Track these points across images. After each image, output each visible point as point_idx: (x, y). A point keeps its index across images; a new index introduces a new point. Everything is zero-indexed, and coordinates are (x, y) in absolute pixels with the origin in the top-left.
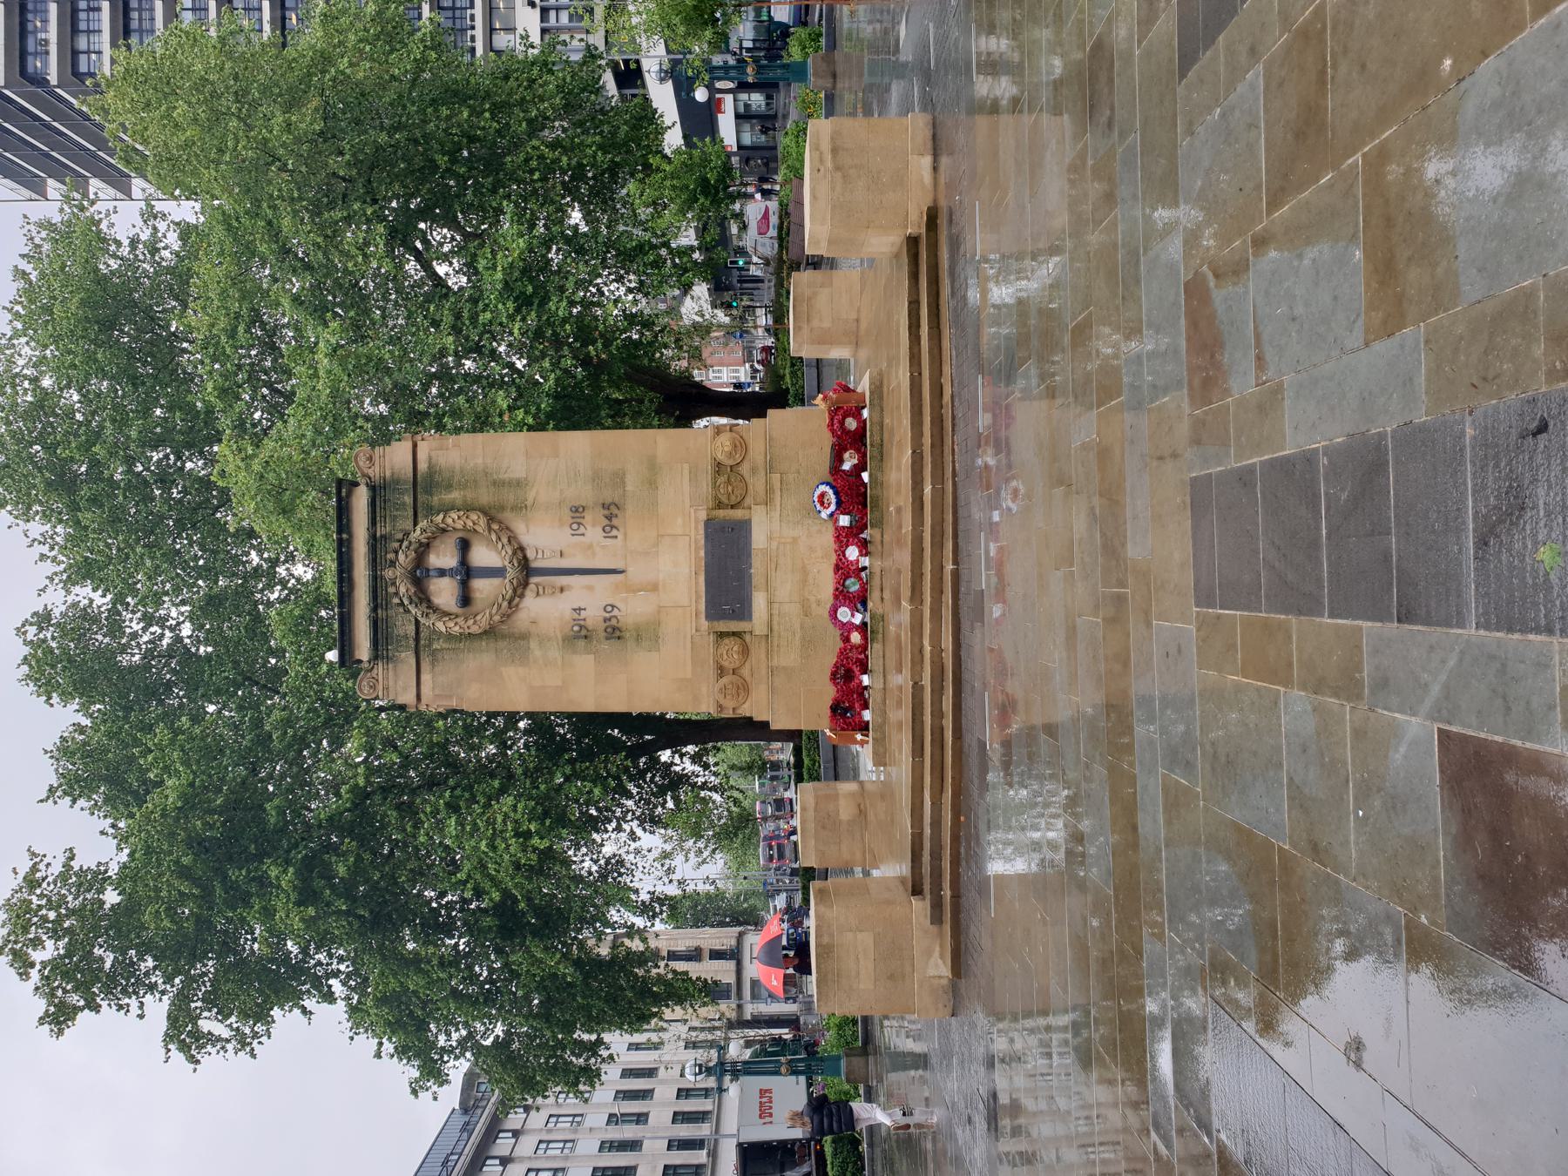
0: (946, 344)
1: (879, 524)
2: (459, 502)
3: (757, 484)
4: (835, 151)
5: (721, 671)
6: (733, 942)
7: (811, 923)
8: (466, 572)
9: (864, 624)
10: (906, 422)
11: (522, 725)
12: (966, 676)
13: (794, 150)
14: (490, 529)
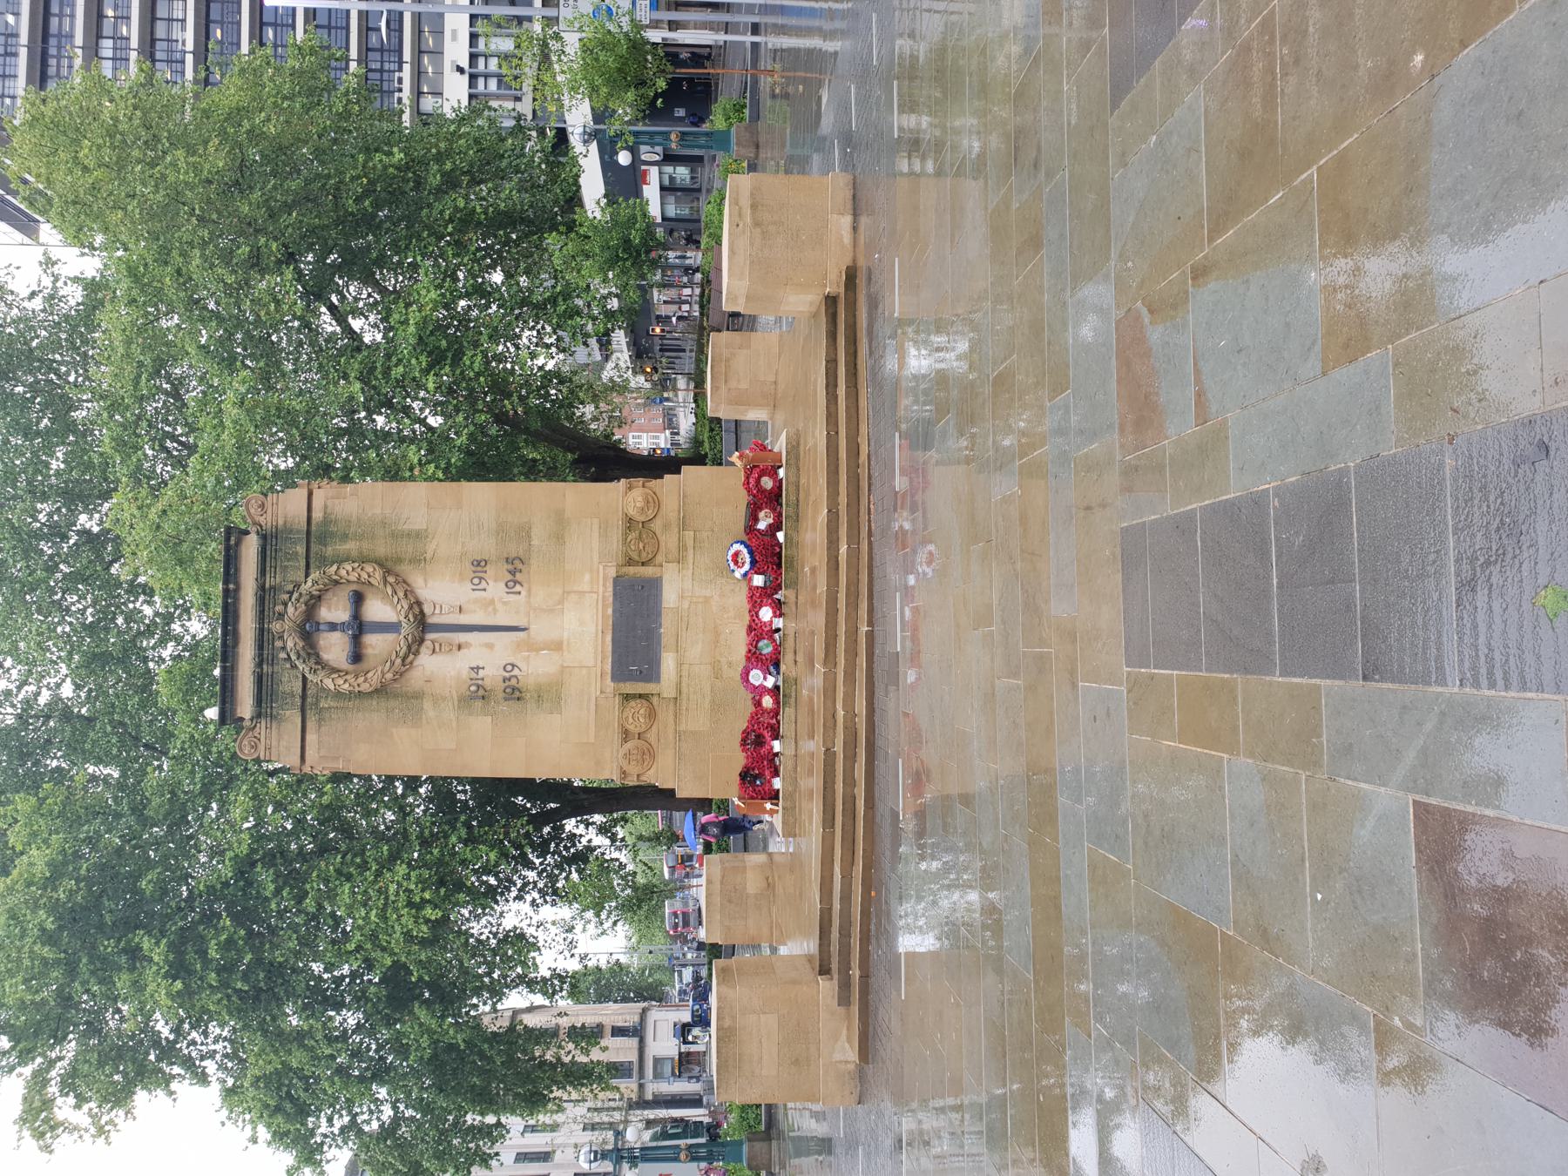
0: (863, 403)
1: (794, 584)
2: (354, 554)
3: (669, 541)
4: (754, 207)
5: (626, 735)
6: (637, 1018)
7: (713, 999)
8: (358, 628)
9: (777, 687)
10: (823, 480)
11: (422, 790)
12: (879, 742)
13: (715, 219)
14: (385, 582)
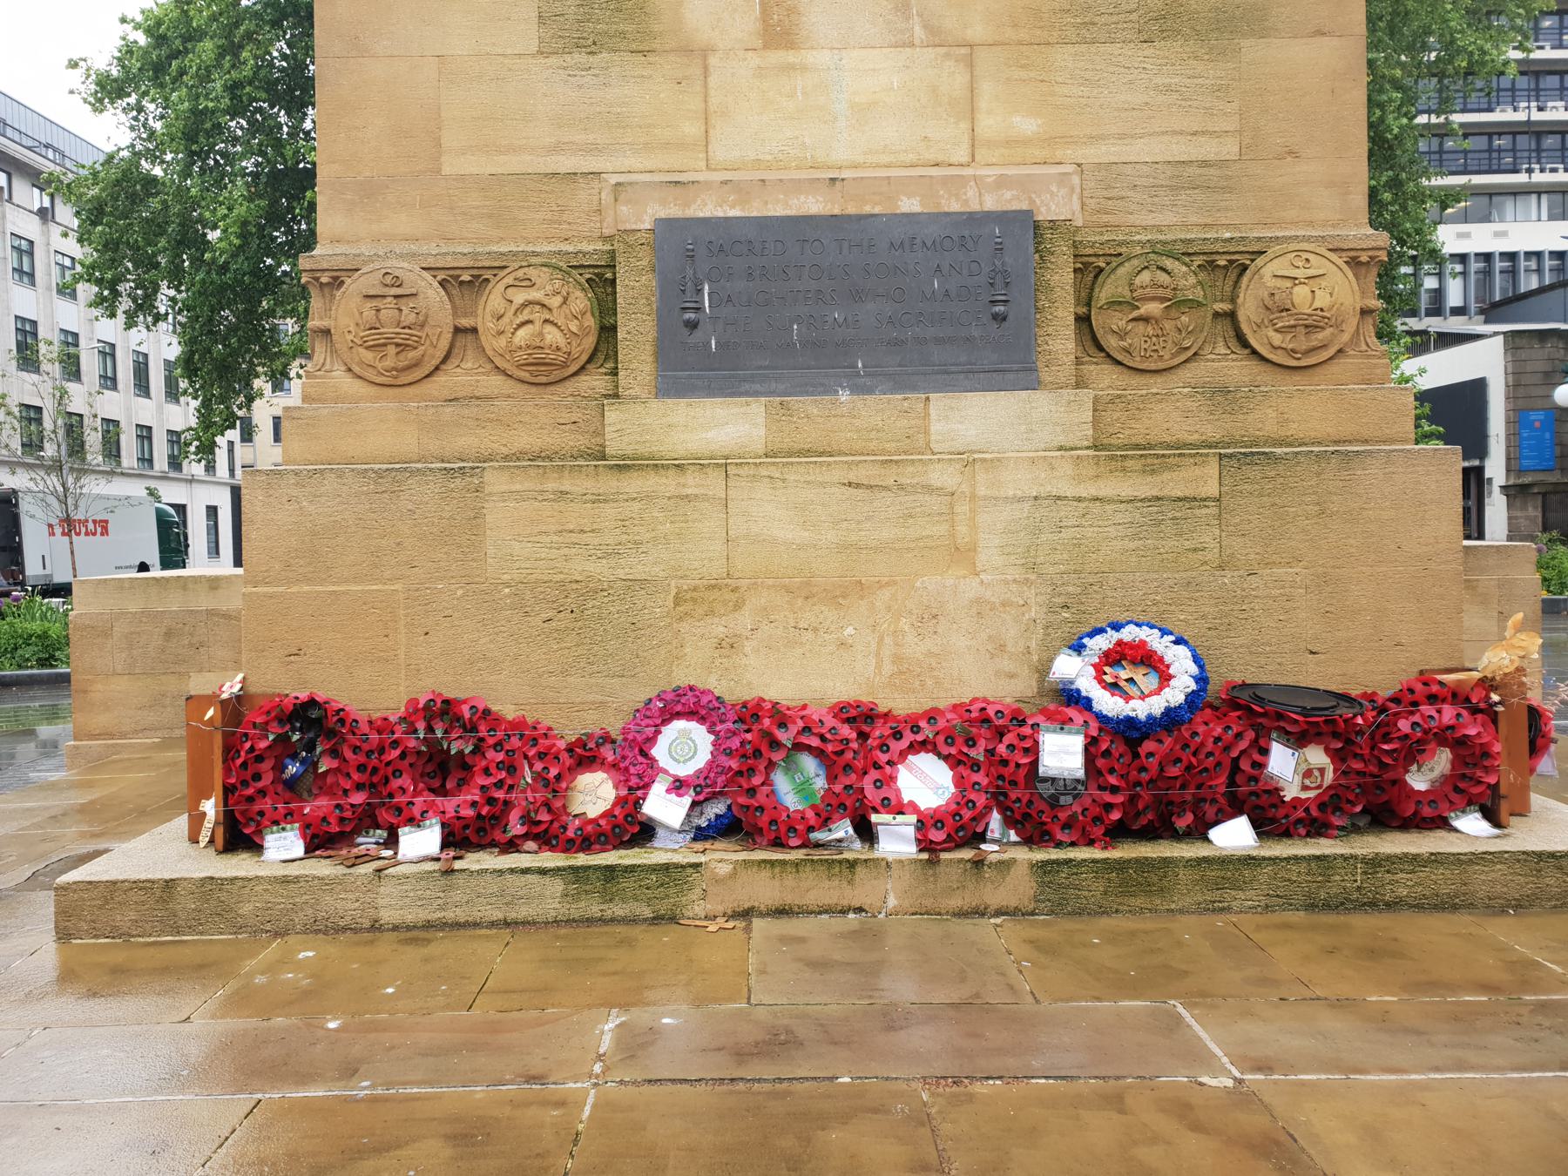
3: (1171, 411)
5: (465, 282)
9: (645, 832)
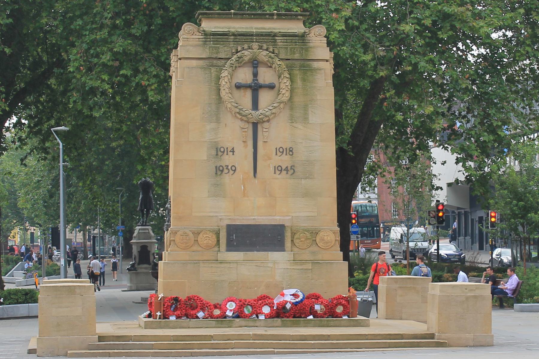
4: (475, 297)
5: (197, 234)
14: (280, 103)
